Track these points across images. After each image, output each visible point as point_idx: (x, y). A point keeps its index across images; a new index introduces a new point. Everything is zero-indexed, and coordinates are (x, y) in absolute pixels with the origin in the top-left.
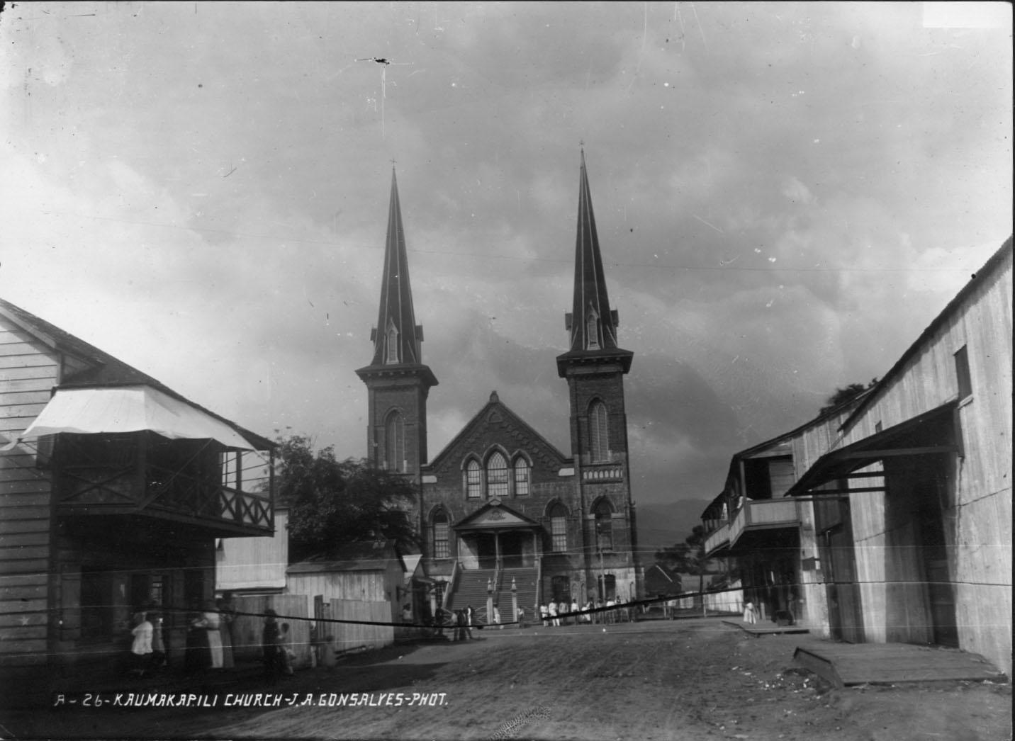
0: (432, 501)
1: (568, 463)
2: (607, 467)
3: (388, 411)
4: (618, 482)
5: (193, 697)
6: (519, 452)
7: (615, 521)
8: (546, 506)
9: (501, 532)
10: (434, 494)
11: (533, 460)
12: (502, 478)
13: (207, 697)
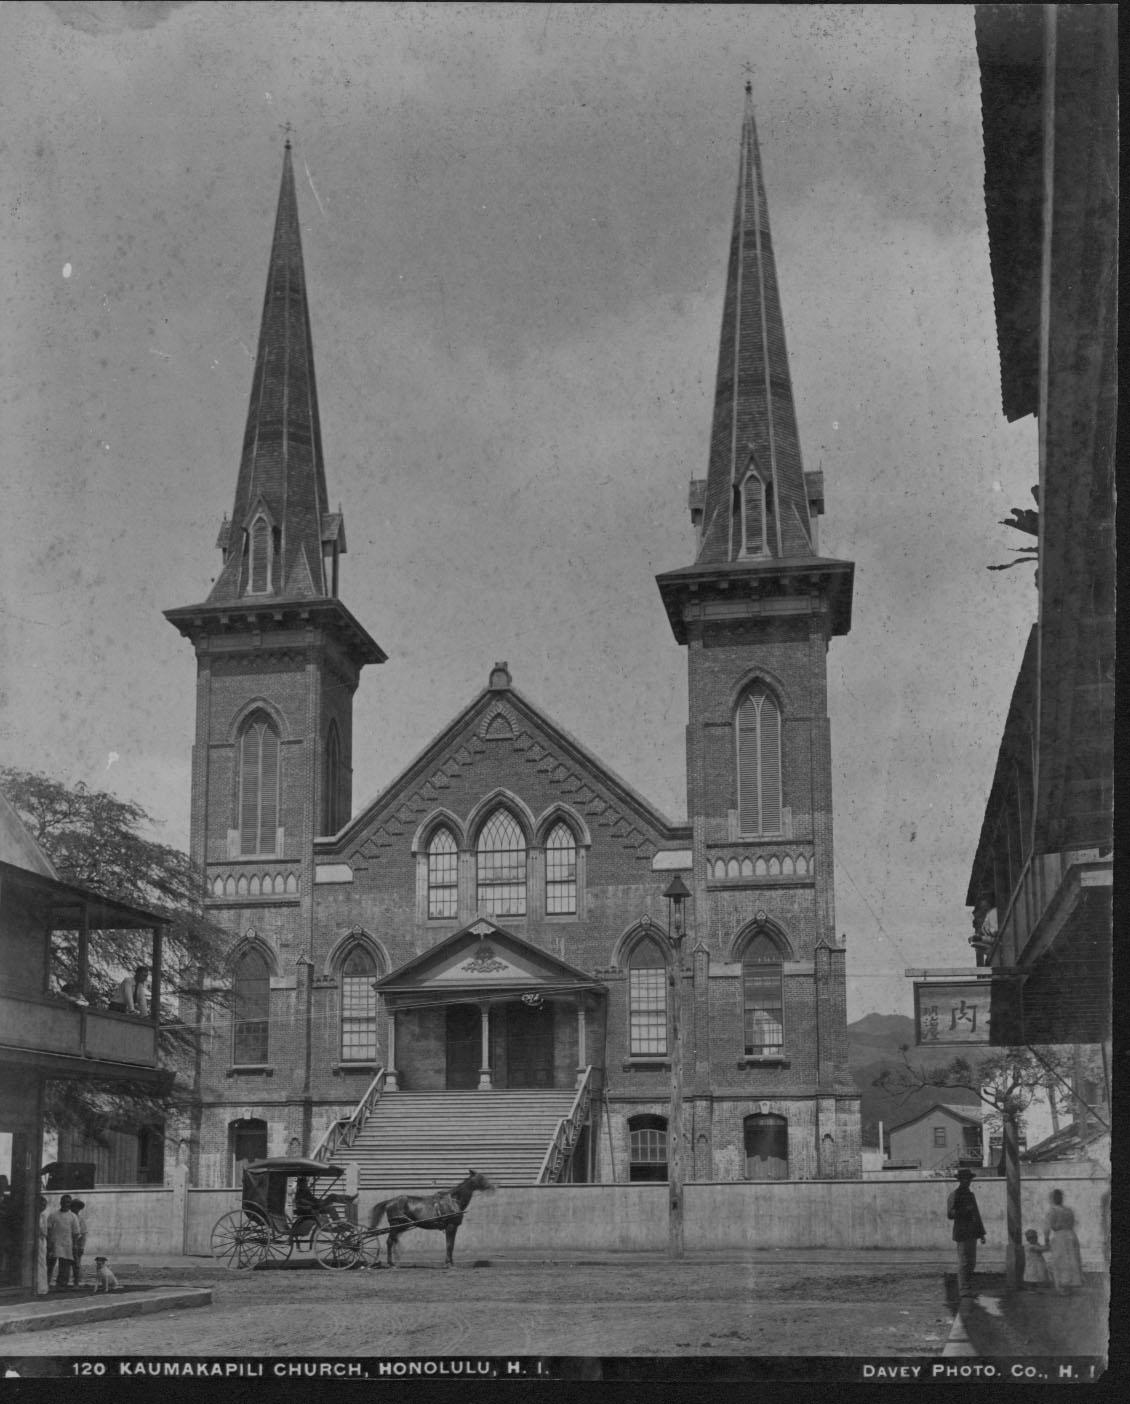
0: (338, 925)
1: (679, 836)
2: (776, 849)
3: (241, 710)
4: (804, 886)
5: (232, 1368)
6: (558, 809)
7: (792, 983)
8: (618, 942)
9: (494, 999)
10: (344, 909)
11: (592, 831)
12: (514, 872)
13: (249, 1366)
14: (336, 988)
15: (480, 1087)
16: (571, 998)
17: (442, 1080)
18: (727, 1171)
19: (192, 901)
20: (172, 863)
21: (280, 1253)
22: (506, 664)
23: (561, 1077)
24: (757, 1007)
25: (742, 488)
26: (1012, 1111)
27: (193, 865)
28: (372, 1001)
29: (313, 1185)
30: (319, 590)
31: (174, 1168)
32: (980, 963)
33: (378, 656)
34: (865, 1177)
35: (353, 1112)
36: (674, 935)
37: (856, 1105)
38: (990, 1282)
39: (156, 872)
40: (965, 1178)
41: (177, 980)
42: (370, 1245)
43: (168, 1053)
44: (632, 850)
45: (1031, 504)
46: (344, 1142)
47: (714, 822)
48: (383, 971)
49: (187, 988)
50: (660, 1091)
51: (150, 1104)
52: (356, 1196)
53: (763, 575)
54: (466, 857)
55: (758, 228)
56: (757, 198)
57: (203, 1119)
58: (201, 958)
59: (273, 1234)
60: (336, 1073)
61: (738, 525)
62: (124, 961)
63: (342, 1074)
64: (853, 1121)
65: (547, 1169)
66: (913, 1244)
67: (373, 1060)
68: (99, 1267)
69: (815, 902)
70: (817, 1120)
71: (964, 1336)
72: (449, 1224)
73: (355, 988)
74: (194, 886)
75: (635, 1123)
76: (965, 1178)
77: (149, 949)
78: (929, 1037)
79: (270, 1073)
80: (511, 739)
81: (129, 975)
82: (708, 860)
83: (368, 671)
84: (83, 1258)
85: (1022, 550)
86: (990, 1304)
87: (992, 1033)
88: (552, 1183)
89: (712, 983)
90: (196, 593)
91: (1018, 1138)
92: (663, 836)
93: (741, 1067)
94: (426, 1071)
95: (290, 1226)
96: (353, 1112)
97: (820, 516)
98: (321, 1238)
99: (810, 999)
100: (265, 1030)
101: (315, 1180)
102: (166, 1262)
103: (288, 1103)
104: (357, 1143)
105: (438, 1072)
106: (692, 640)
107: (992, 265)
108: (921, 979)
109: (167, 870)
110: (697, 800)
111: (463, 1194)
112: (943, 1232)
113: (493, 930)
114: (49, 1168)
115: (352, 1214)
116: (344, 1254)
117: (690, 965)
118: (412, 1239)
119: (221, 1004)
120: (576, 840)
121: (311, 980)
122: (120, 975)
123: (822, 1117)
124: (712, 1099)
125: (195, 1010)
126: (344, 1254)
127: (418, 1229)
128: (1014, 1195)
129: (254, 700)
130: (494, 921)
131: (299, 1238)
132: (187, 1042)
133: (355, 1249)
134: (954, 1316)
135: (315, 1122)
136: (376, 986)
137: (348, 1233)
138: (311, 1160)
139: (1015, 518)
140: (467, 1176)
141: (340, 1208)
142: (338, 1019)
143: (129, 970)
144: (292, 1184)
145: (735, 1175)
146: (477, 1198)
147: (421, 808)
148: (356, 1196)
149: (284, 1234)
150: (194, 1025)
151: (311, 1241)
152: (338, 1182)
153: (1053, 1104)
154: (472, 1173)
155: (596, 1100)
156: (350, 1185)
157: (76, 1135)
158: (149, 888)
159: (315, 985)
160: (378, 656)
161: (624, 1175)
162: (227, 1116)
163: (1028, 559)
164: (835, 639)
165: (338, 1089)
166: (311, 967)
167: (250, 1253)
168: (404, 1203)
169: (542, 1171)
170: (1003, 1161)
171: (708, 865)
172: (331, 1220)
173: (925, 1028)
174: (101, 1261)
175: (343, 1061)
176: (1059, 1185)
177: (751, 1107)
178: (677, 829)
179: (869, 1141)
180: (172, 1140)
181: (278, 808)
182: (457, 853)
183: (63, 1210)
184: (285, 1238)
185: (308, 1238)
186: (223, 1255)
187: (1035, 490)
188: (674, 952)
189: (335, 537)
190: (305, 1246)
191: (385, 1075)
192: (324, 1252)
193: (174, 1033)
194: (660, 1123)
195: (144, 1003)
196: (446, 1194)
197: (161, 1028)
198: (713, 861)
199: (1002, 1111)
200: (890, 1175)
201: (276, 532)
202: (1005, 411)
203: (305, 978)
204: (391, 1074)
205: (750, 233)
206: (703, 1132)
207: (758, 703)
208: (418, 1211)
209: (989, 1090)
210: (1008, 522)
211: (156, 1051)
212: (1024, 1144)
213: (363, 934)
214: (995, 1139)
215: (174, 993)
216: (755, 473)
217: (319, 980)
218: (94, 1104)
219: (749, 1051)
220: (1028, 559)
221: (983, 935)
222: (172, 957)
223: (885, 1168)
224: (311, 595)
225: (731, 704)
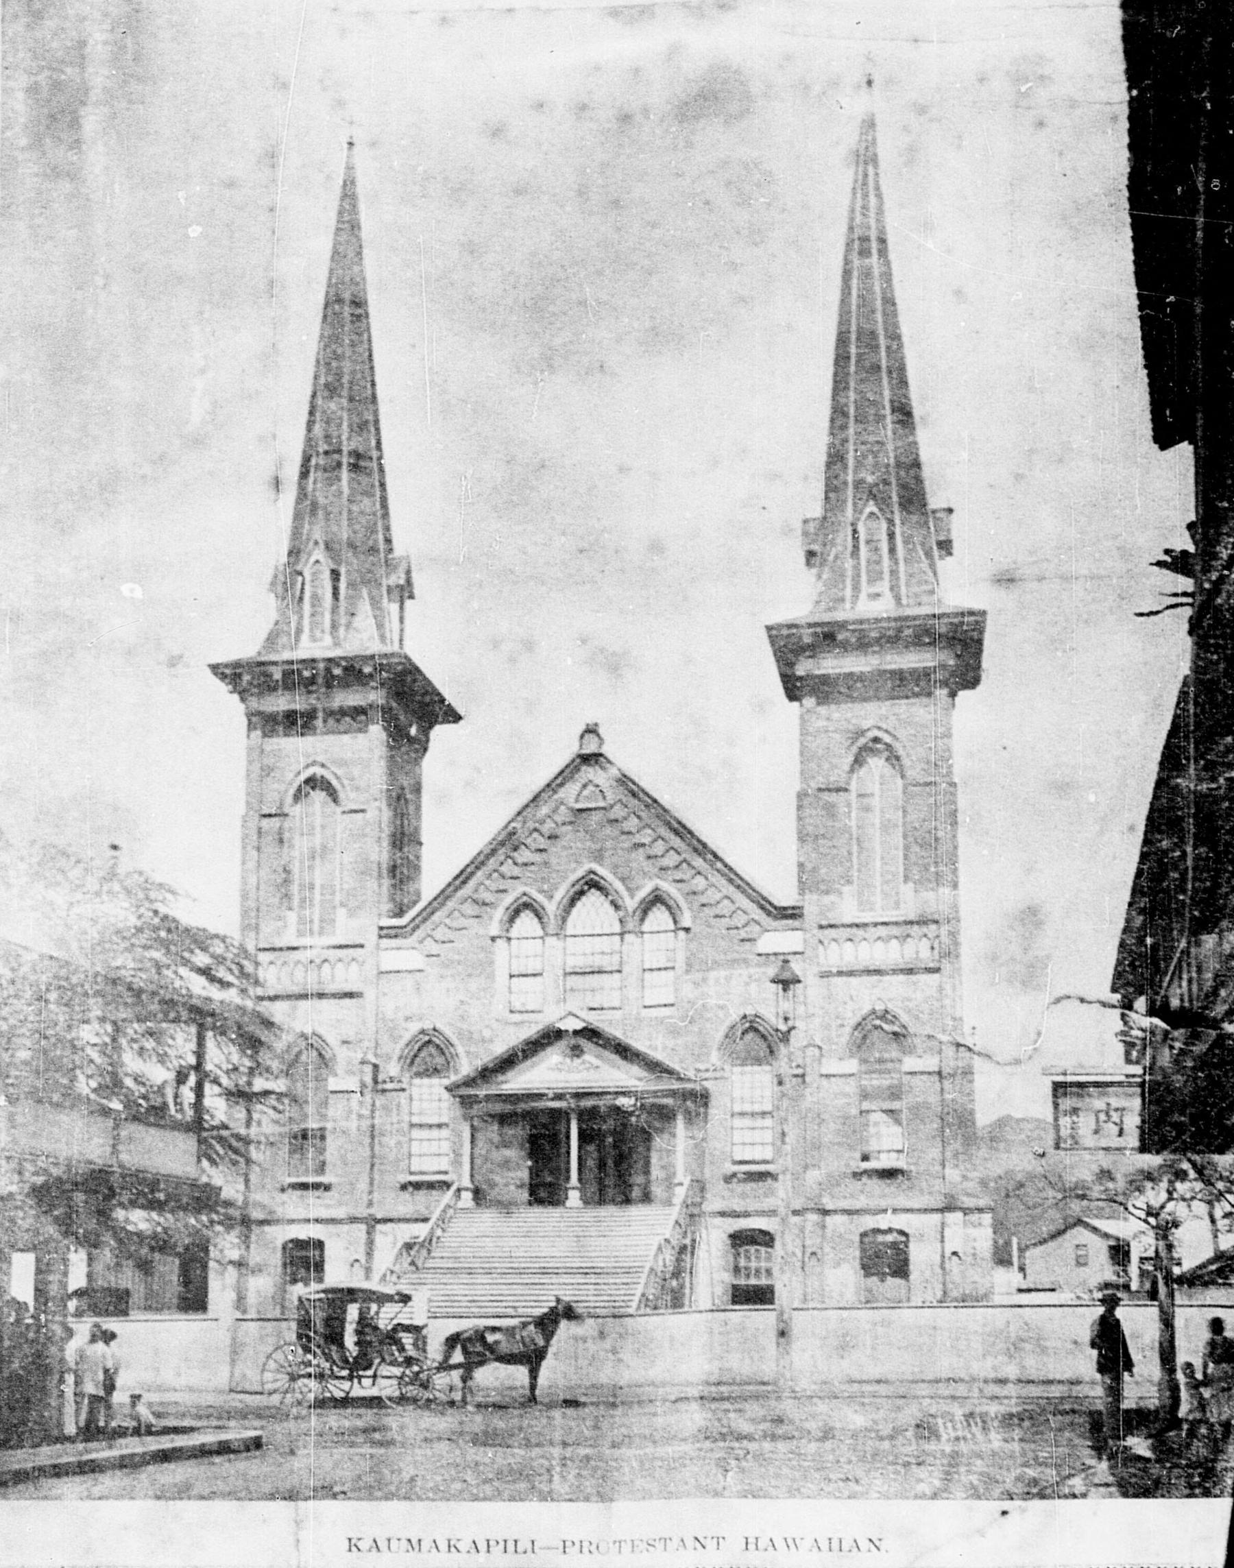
7: (917, 1081)
14: (403, 1090)
15: (568, 1204)
16: (669, 1101)
17: (525, 1195)
18: (841, 1295)
19: (243, 991)
20: (218, 948)
21: (337, 1389)
22: (596, 725)
23: (657, 1190)
24: (874, 1108)
25: (861, 528)
26: (1165, 1230)
27: (243, 950)
28: (445, 1105)
29: (377, 1313)
30: (383, 638)
31: (220, 1290)
32: (1128, 1061)
33: (453, 716)
34: (997, 1300)
35: (421, 1230)
36: (783, 1028)
37: (987, 1218)
38: (1138, 1419)
39: (201, 959)
40: (1111, 1303)
41: (225, 1081)
42: (441, 1381)
43: (213, 1162)
44: (735, 931)
45: (1184, 543)
46: (413, 1263)
47: (827, 899)
48: (456, 1071)
49: (234, 1090)
50: (769, 1203)
51: (192, 1221)
52: (426, 1326)
53: (885, 625)
54: (551, 941)
55: (873, 235)
56: (873, 200)
57: (253, 1238)
58: (252, 1056)
59: (332, 1370)
60: (404, 1187)
61: (857, 567)
62: (162, 1059)
63: (411, 1189)
64: (982, 1236)
65: (643, 1295)
66: (1051, 1377)
67: (446, 1173)
68: (133, 1405)
69: (941, 989)
70: (943, 1237)
71: (1111, 1479)
72: (533, 1358)
73: (425, 1090)
74: (243, 974)
75: (739, 1239)
76: (1111, 1303)
77: (193, 1046)
78: (1069, 1142)
79: (327, 1188)
80: (604, 808)
81: (171, 1076)
82: (821, 942)
83: (440, 733)
84: (115, 1394)
85: (1176, 595)
86: (1140, 1445)
87: (1142, 1139)
88: (648, 1311)
89: (824, 1082)
90: (246, 648)
91: (1172, 1259)
92: (769, 914)
93: (857, 1175)
94: (506, 1185)
95: (351, 1360)
96: (421, 1230)
97: (949, 559)
98: (385, 1373)
99: (933, 1099)
100: (323, 1138)
101: (379, 1308)
102: (210, 1399)
103: (353, 1220)
104: (427, 1265)
105: (521, 1186)
106: (803, 696)
107: (1137, 273)
108: (1060, 1079)
109: (213, 956)
110: (807, 879)
111: (547, 1323)
112: (1086, 1364)
113: (584, 1025)
114: (79, 1293)
115: (420, 1343)
116: (411, 1391)
117: (800, 1061)
118: (490, 1376)
119: (274, 1108)
120: (675, 922)
121: (376, 1081)
122: (160, 1074)
123: (947, 1232)
124: (826, 1212)
125: (244, 1112)
126: (411, 1391)
127: (497, 1364)
128: (1167, 1323)
129: (314, 763)
130: (584, 1014)
131: (361, 1373)
132: (236, 1152)
133: (425, 1386)
134: (1100, 1459)
135: (379, 1239)
136: (448, 1089)
137: (416, 1368)
138: (373, 1285)
139: (1169, 559)
140: (553, 1304)
141: (407, 1339)
142: (405, 1126)
143: (168, 1069)
144: (353, 1312)
145: (850, 1297)
146: (565, 1328)
147: (501, 888)
148: (426, 1326)
149: (343, 1368)
150: (243, 1131)
151: (375, 1376)
152: (406, 1309)
153: (1213, 1221)
154: (558, 1300)
155: (693, 1215)
156: (416, 1314)
157: (106, 1255)
158: (194, 976)
159: (380, 1087)
160: (453, 716)
161: (725, 1298)
162: (281, 1234)
163: (1182, 605)
164: (962, 694)
165: (406, 1204)
166: (376, 1066)
167: (305, 1390)
168: (480, 1336)
169: (636, 1299)
170: (1154, 1283)
171: (821, 947)
172: (397, 1353)
173: (1065, 1132)
174: (136, 1398)
175: (411, 1173)
176: (1219, 1313)
177: (869, 1222)
178: (785, 908)
179: (1002, 1258)
180: (217, 1261)
181: (338, 887)
182: (542, 938)
183: (93, 1339)
184: (345, 1373)
185: (370, 1373)
186: (275, 1391)
187: (1191, 527)
188: (782, 1045)
189: (402, 582)
190: (367, 1382)
191: (459, 1190)
192: (387, 1388)
193: (221, 1139)
194: (764, 1239)
195: (186, 1107)
196: (530, 1323)
197: (205, 1134)
198: (826, 942)
199: (1153, 1227)
200: (1025, 1299)
201: (335, 575)
202: (1156, 439)
203: (368, 1079)
204: (467, 1189)
205: (865, 239)
206: (814, 1249)
207: (876, 764)
208: (497, 1342)
209: (1138, 1204)
210: (1159, 564)
211: (199, 1161)
212: (1179, 1264)
213: (435, 1029)
214: (1146, 1259)
215: (220, 1095)
216: (875, 510)
217: (384, 1082)
218: (127, 1220)
219: (865, 1158)
220: (1182, 605)
221: (1132, 1028)
222: (220, 1055)
223: (1020, 1291)
224: (375, 647)
225: (847, 768)
